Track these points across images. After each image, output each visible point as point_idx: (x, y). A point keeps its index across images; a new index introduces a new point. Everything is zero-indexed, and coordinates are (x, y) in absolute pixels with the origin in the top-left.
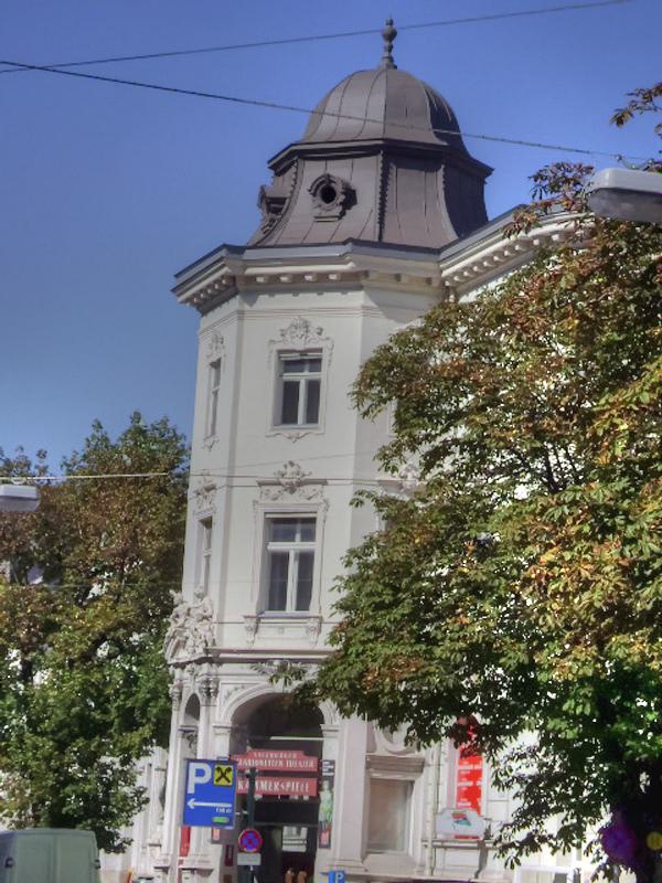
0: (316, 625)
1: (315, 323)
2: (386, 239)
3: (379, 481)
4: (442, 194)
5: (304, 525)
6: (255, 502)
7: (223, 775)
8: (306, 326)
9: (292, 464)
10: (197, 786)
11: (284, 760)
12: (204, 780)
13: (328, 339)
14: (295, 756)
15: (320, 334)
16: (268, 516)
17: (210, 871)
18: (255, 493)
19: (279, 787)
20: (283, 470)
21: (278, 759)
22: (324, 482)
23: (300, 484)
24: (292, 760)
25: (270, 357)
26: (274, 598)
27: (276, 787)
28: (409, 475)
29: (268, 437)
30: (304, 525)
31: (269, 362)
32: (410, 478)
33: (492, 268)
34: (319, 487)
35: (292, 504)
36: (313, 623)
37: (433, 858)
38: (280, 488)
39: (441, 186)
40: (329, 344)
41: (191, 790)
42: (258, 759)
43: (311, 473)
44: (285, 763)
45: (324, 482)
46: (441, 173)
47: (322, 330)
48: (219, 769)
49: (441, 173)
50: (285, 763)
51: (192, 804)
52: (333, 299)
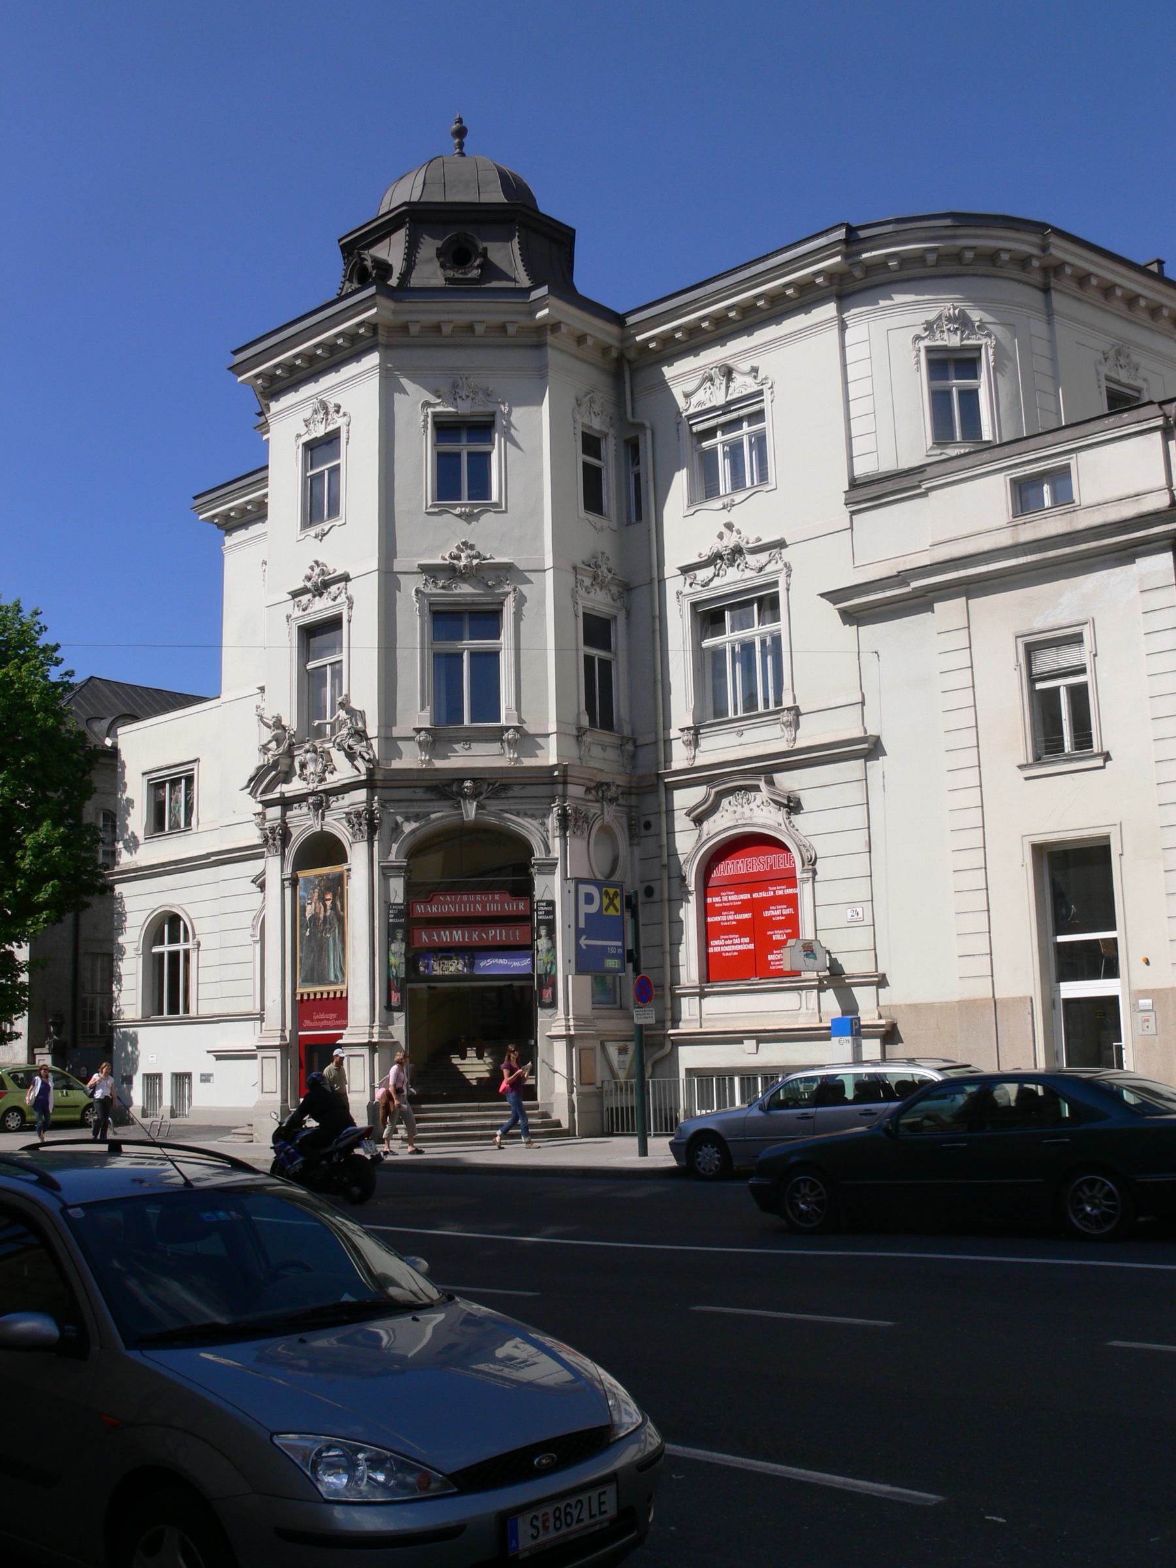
1: (332, 401)
3: (420, 566)
4: (518, 259)
5: (486, 620)
6: (288, 617)
7: (611, 903)
8: (324, 406)
10: (587, 916)
12: (593, 908)
13: (345, 415)
14: (497, 897)
15: (338, 412)
18: (419, 581)
25: (917, 356)
27: (475, 936)
28: (463, 555)
29: (429, 514)
31: (918, 362)
33: (325, 359)
34: (342, 584)
35: (321, 608)
38: (309, 596)
39: (517, 252)
40: (345, 419)
41: (582, 925)
43: (335, 571)
44: (484, 907)
46: (516, 240)
47: (339, 407)
48: (607, 893)
49: (516, 240)
50: (484, 907)
51: (583, 942)
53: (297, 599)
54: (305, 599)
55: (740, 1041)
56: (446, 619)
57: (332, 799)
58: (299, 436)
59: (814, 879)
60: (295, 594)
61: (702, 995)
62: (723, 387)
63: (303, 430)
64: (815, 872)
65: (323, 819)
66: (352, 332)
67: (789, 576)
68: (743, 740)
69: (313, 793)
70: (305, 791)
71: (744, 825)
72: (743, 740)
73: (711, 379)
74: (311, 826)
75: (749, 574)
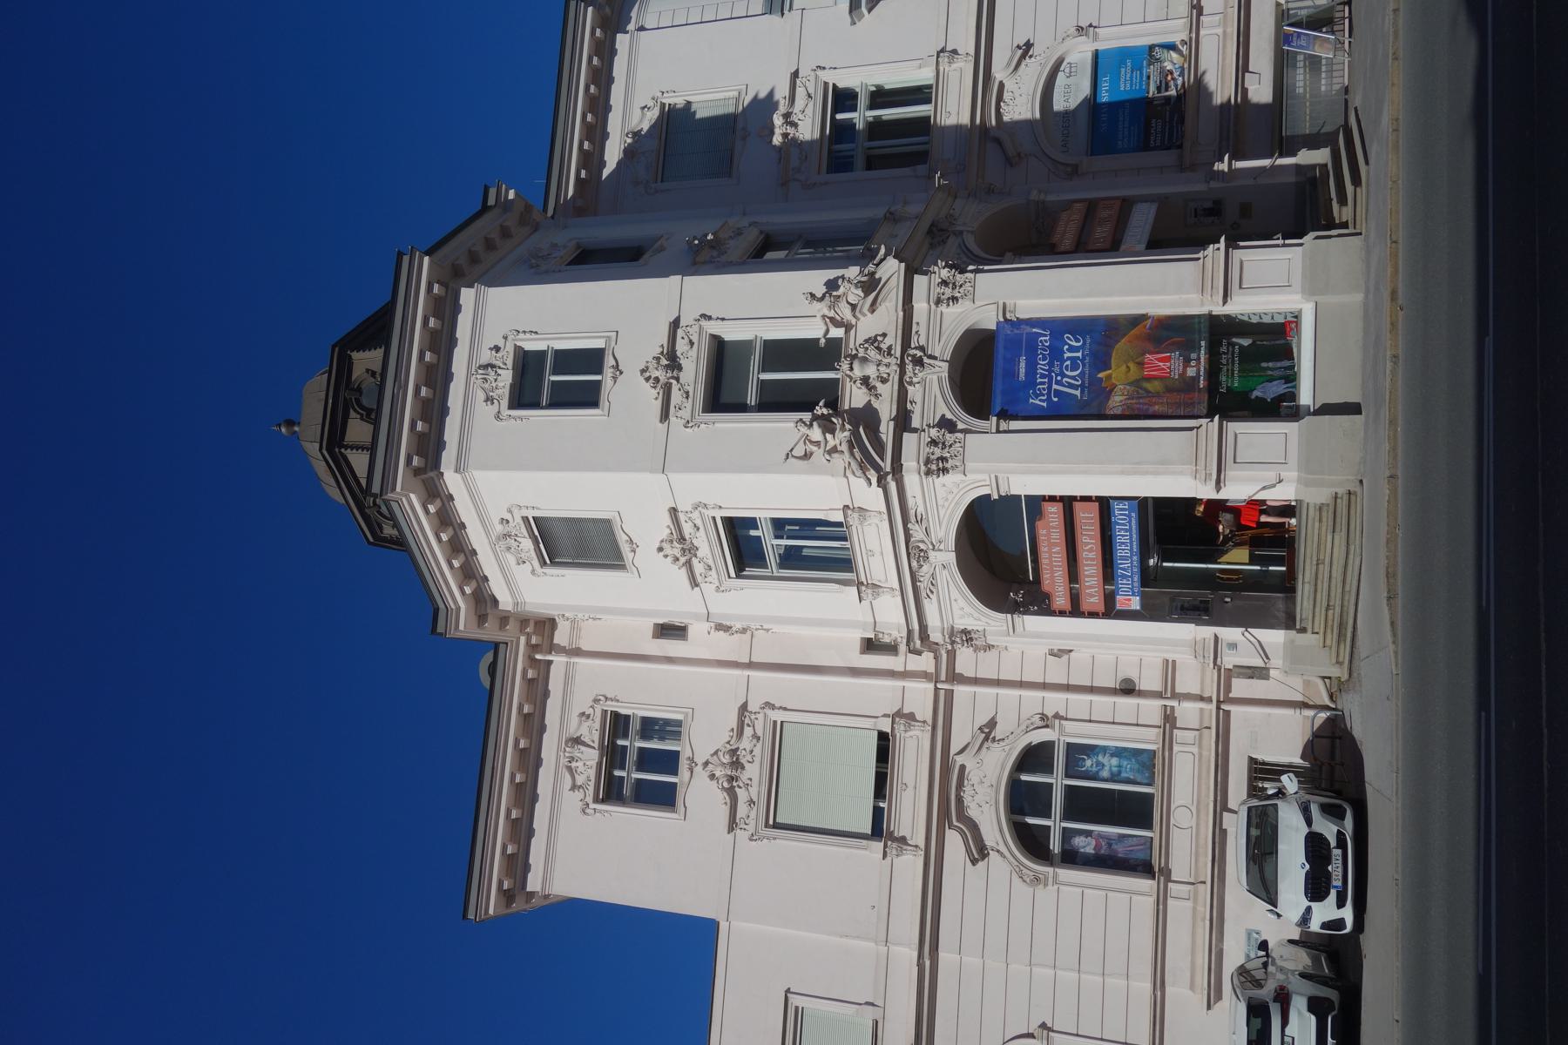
0: (856, 515)
2: (368, 444)
5: (723, 356)
9: (660, 549)
11: (1051, 545)
16: (733, 574)
17: (1216, 637)
19: (1090, 550)
20: (669, 559)
21: (1050, 552)
22: (674, 511)
23: (682, 539)
24: (1051, 529)
26: (840, 564)
27: (1091, 555)
30: (723, 356)
32: (657, 374)
34: (682, 517)
35: (711, 549)
36: (854, 519)
37: (845, 516)
38: (695, 561)
40: (515, 511)
42: (1052, 577)
45: (674, 511)
50: (1056, 545)
52: (464, 509)
53: (699, 579)
54: (698, 568)
55: (1224, 832)
56: (721, 396)
57: (914, 338)
58: (533, 572)
59: (1062, 718)
60: (694, 583)
61: (1166, 873)
62: (583, 748)
63: (527, 567)
64: (1057, 716)
65: (935, 358)
66: (436, 521)
67: (710, 318)
68: (911, 784)
69: (902, 366)
70: (896, 387)
71: (997, 803)
72: (911, 784)
73: (572, 759)
74: (940, 380)
75: (809, 111)
